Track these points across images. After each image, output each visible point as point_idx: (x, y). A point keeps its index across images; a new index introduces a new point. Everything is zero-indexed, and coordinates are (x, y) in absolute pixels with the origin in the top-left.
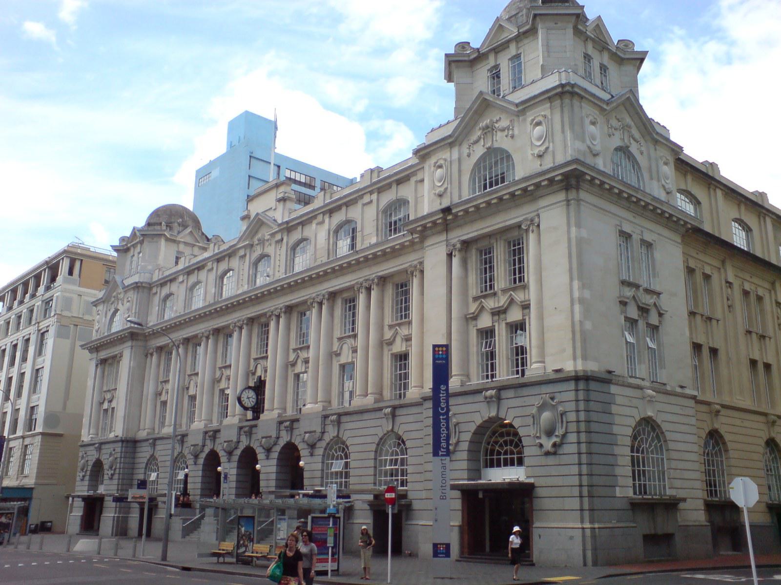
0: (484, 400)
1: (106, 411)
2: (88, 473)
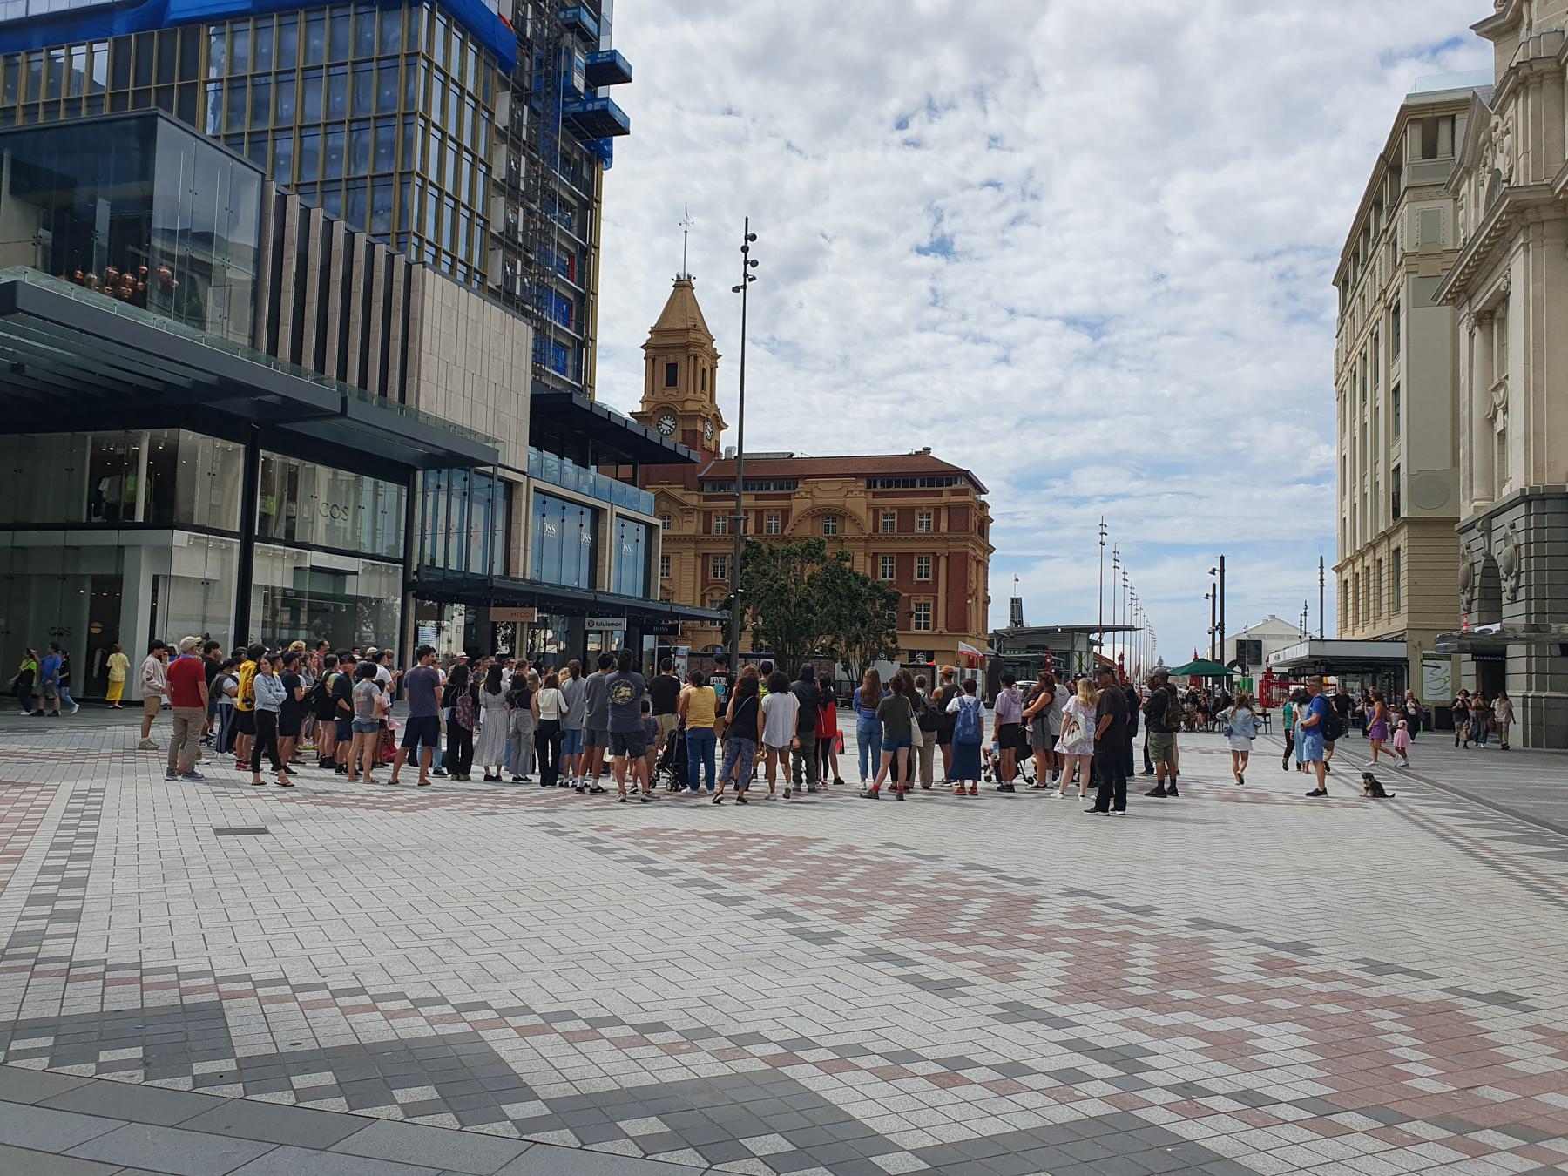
0: (1233, 631)
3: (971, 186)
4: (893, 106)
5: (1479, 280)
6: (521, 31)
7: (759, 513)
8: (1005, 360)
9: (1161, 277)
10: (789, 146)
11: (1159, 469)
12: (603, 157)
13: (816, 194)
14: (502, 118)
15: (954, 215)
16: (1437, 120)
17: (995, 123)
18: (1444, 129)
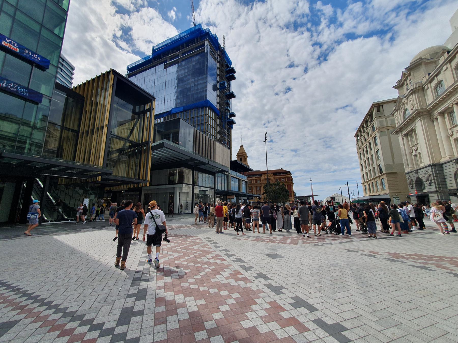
1: (415, 156)
2: (414, 185)
3: (275, 132)
4: (263, 122)
5: (404, 128)
6: (220, 110)
7: (256, 180)
8: (282, 157)
9: (305, 143)
10: (248, 129)
11: (308, 171)
12: (231, 128)
13: (253, 135)
14: (218, 123)
15: (273, 136)
16: (379, 106)
17: (278, 123)
18: (381, 108)
